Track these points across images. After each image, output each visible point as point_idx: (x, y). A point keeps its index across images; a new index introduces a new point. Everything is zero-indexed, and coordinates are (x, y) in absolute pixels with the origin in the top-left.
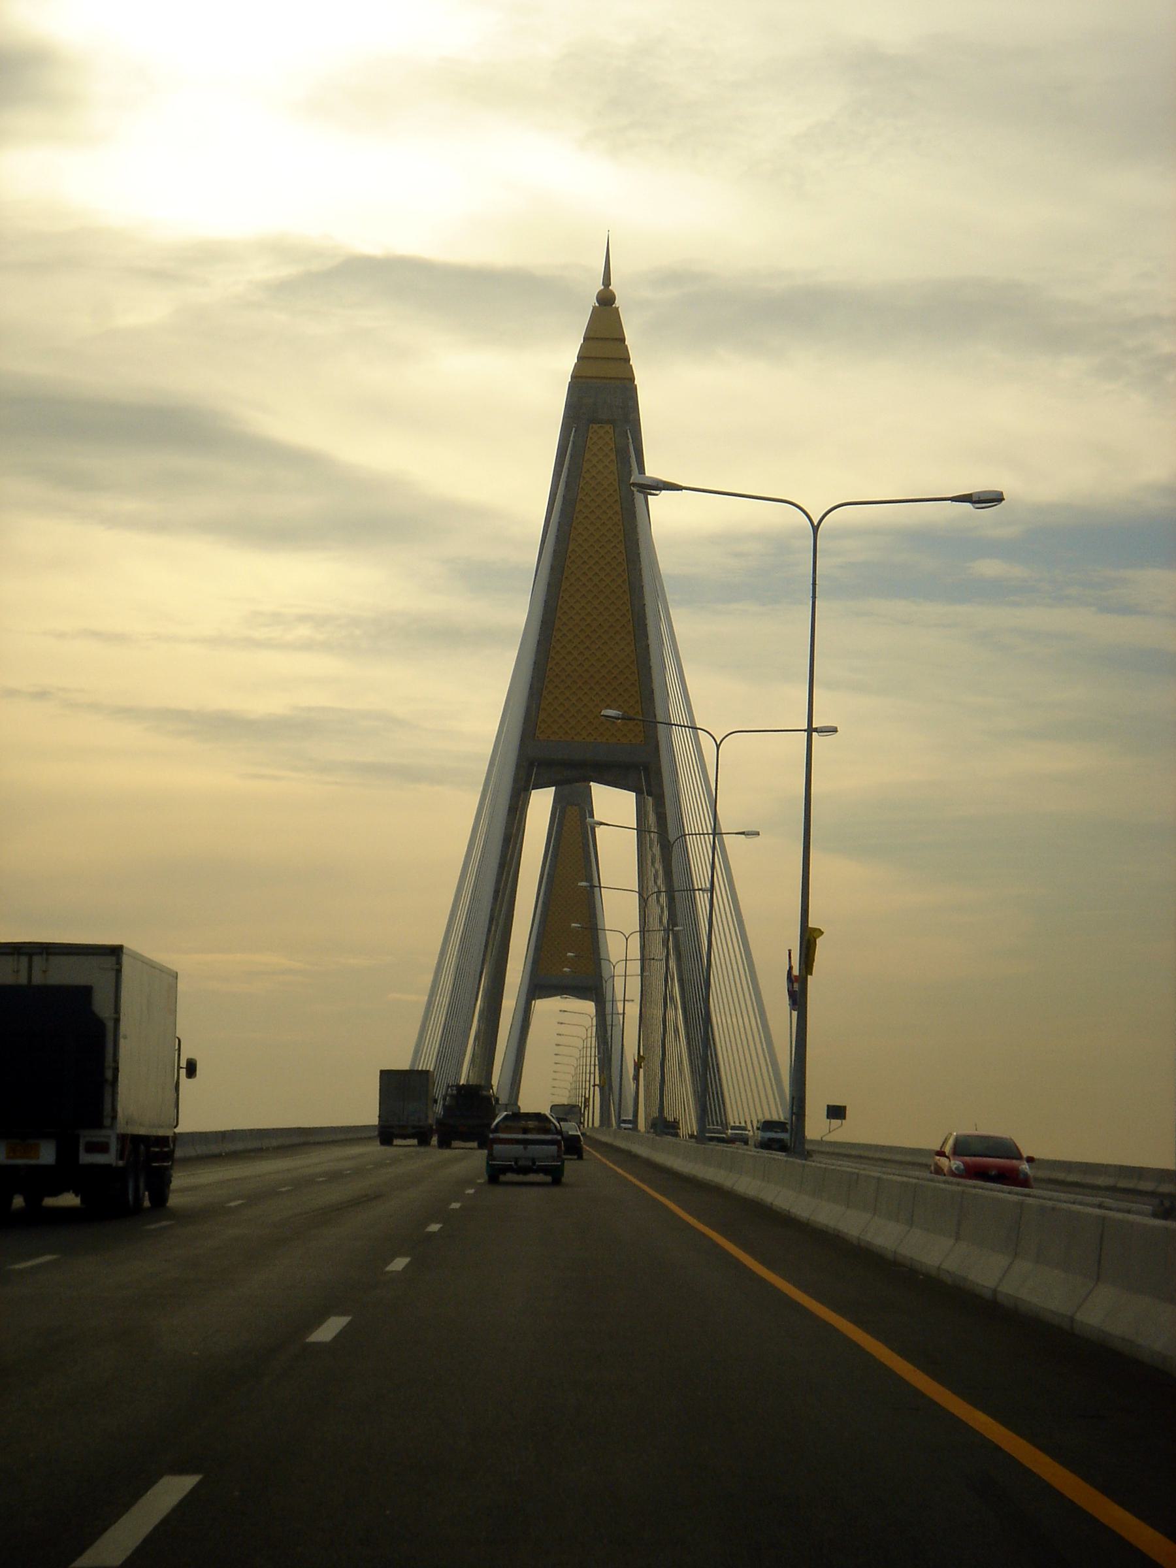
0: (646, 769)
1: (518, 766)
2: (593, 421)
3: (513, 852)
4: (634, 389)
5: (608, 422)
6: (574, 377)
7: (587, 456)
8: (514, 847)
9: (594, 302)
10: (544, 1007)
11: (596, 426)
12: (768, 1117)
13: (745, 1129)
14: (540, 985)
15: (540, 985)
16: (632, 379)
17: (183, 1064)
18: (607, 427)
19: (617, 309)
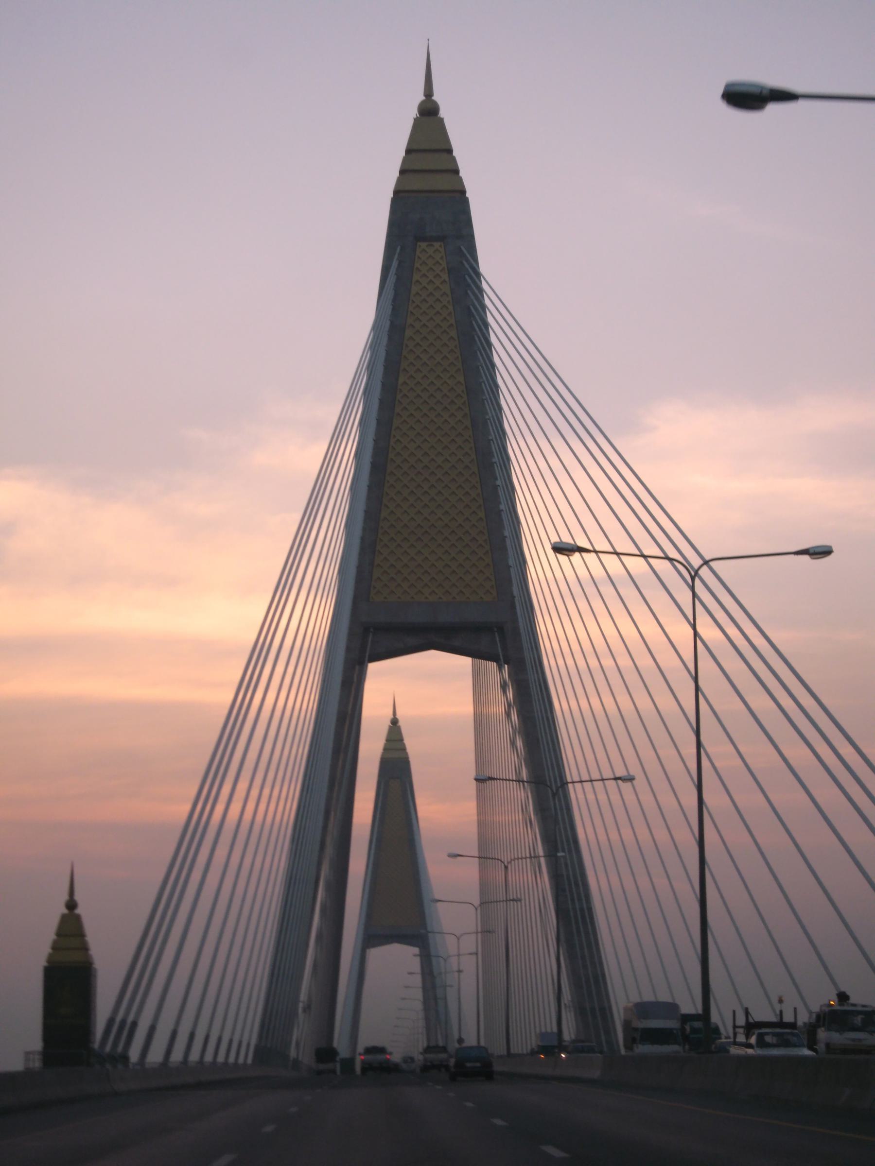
0: (501, 629)
1: (351, 634)
2: (420, 238)
3: (349, 733)
4: (466, 202)
5: (441, 238)
6: (396, 193)
7: (416, 277)
8: (351, 724)
9: (414, 113)
10: (377, 955)
11: (423, 245)
12: (648, 997)
13: (444, 1049)
14: (373, 937)
15: (373, 937)
16: (463, 192)
17: (322, 1066)
18: (437, 245)
19: (442, 120)
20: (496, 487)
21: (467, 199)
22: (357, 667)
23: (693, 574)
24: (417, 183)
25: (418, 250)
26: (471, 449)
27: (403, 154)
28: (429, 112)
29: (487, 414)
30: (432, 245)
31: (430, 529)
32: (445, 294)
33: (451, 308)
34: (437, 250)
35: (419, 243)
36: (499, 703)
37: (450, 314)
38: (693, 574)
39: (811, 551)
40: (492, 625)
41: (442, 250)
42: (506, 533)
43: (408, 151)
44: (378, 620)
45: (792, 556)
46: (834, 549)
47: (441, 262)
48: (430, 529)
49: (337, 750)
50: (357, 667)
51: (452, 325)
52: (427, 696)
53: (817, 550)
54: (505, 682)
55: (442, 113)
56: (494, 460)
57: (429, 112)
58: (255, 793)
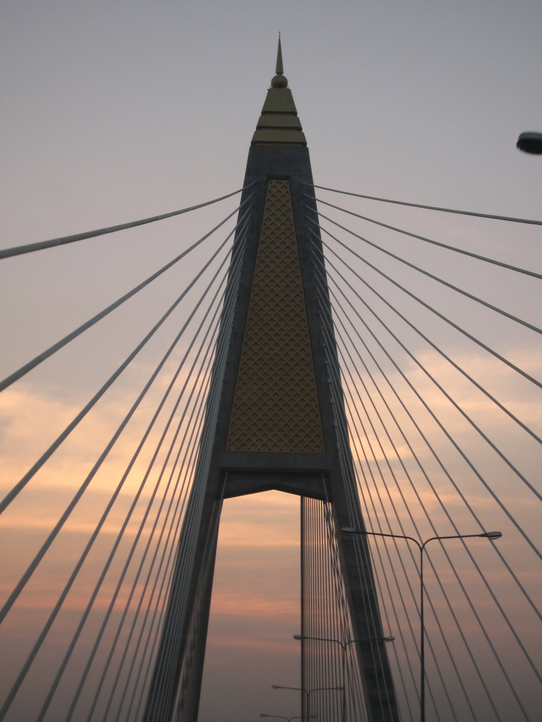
4: (307, 150)
6: (253, 143)
9: (269, 85)
11: (274, 182)
16: (305, 144)
18: (284, 182)
19: (289, 91)
20: (328, 384)
21: (308, 148)
22: (215, 503)
23: (421, 546)
24: (270, 136)
25: (270, 186)
26: (316, 406)
27: (260, 114)
28: (279, 84)
29: (324, 342)
30: (280, 182)
31: (276, 410)
32: (293, 252)
33: (298, 263)
34: (284, 186)
35: (270, 181)
36: (323, 540)
37: (292, 225)
38: (421, 546)
39: (489, 535)
40: (319, 468)
41: (288, 186)
42: (333, 400)
43: (264, 113)
44: (230, 464)
45: (478, 537)
46: (502, 534)
47: (286, 194)
48: (276, 410)
49: (197, 565)
50: (215, 503)
51: (308, 344)
52: (264, 523)
53: (493, 534)
54: (329, 514)
55: (290, 86)
56: (327, 362)
57: (279, 84)
58: (157, 592)
